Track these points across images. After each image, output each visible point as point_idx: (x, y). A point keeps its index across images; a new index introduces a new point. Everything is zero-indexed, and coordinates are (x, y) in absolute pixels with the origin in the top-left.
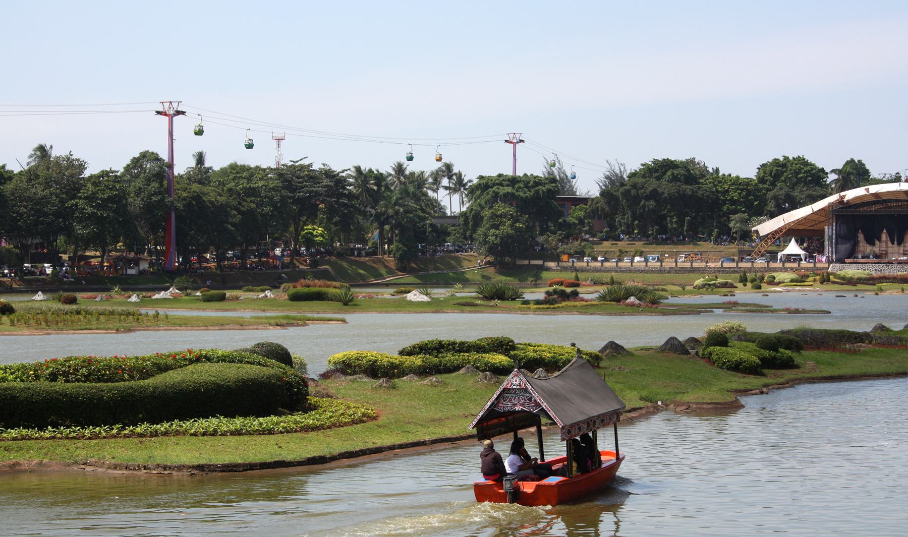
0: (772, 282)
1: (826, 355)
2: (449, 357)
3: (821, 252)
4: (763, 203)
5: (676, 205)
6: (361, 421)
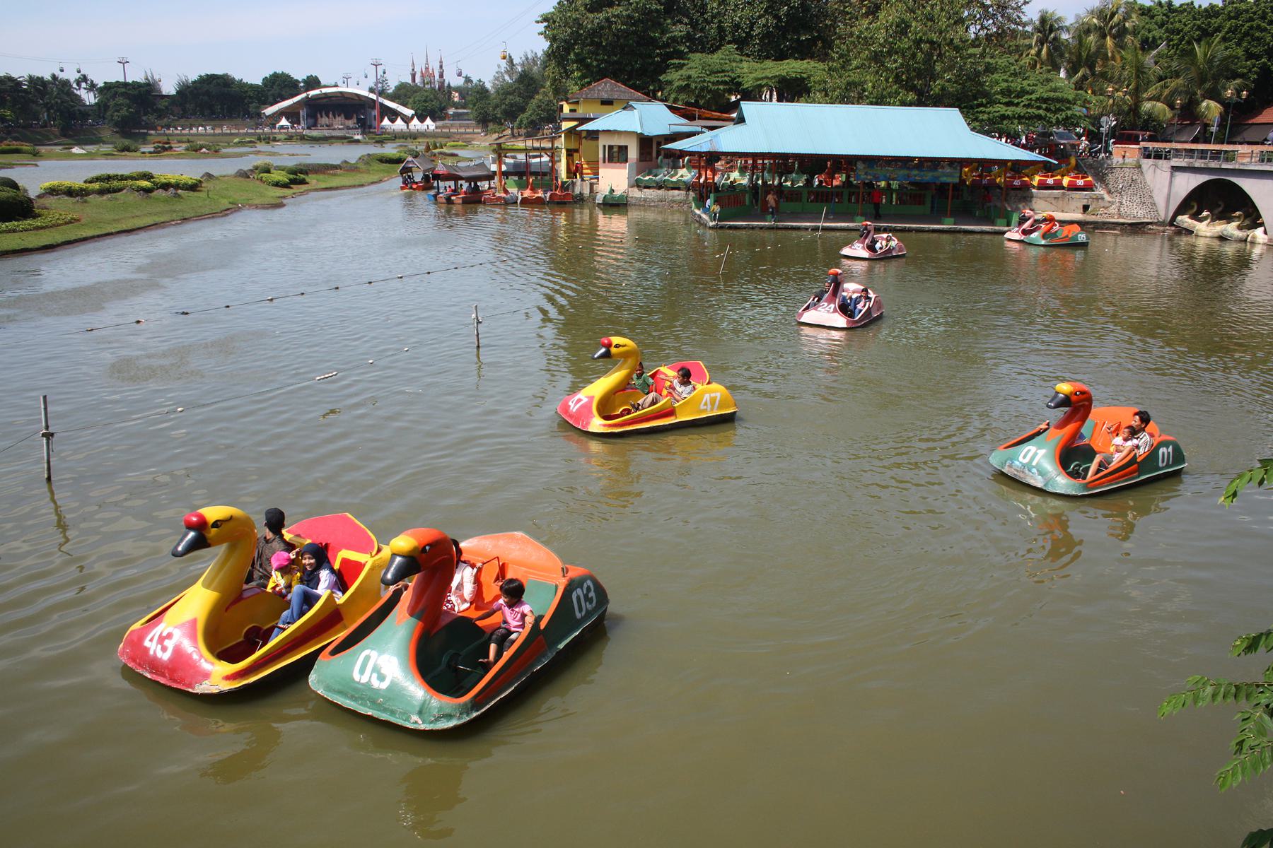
0: (275, 140)
1: (321, 177)
2: (115, 184)
3: (299, 123)
4: (267, 97)
5: (217, 100)
6: (70, 222)
